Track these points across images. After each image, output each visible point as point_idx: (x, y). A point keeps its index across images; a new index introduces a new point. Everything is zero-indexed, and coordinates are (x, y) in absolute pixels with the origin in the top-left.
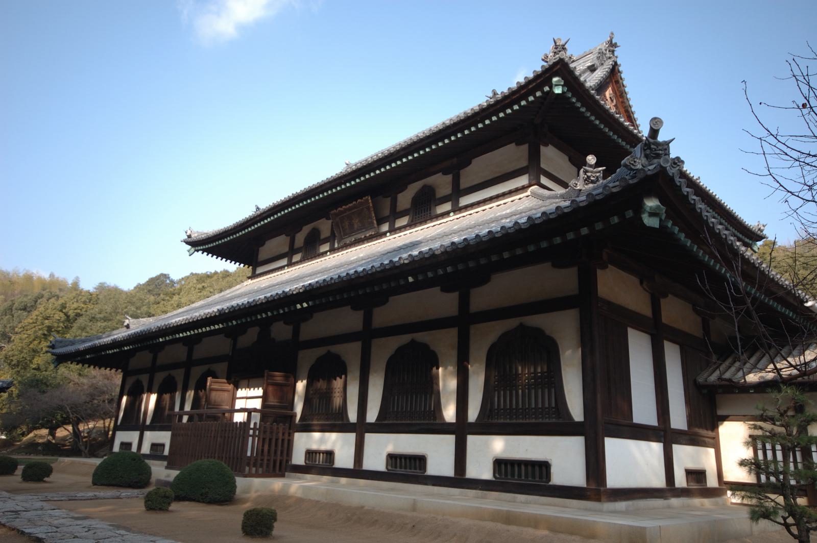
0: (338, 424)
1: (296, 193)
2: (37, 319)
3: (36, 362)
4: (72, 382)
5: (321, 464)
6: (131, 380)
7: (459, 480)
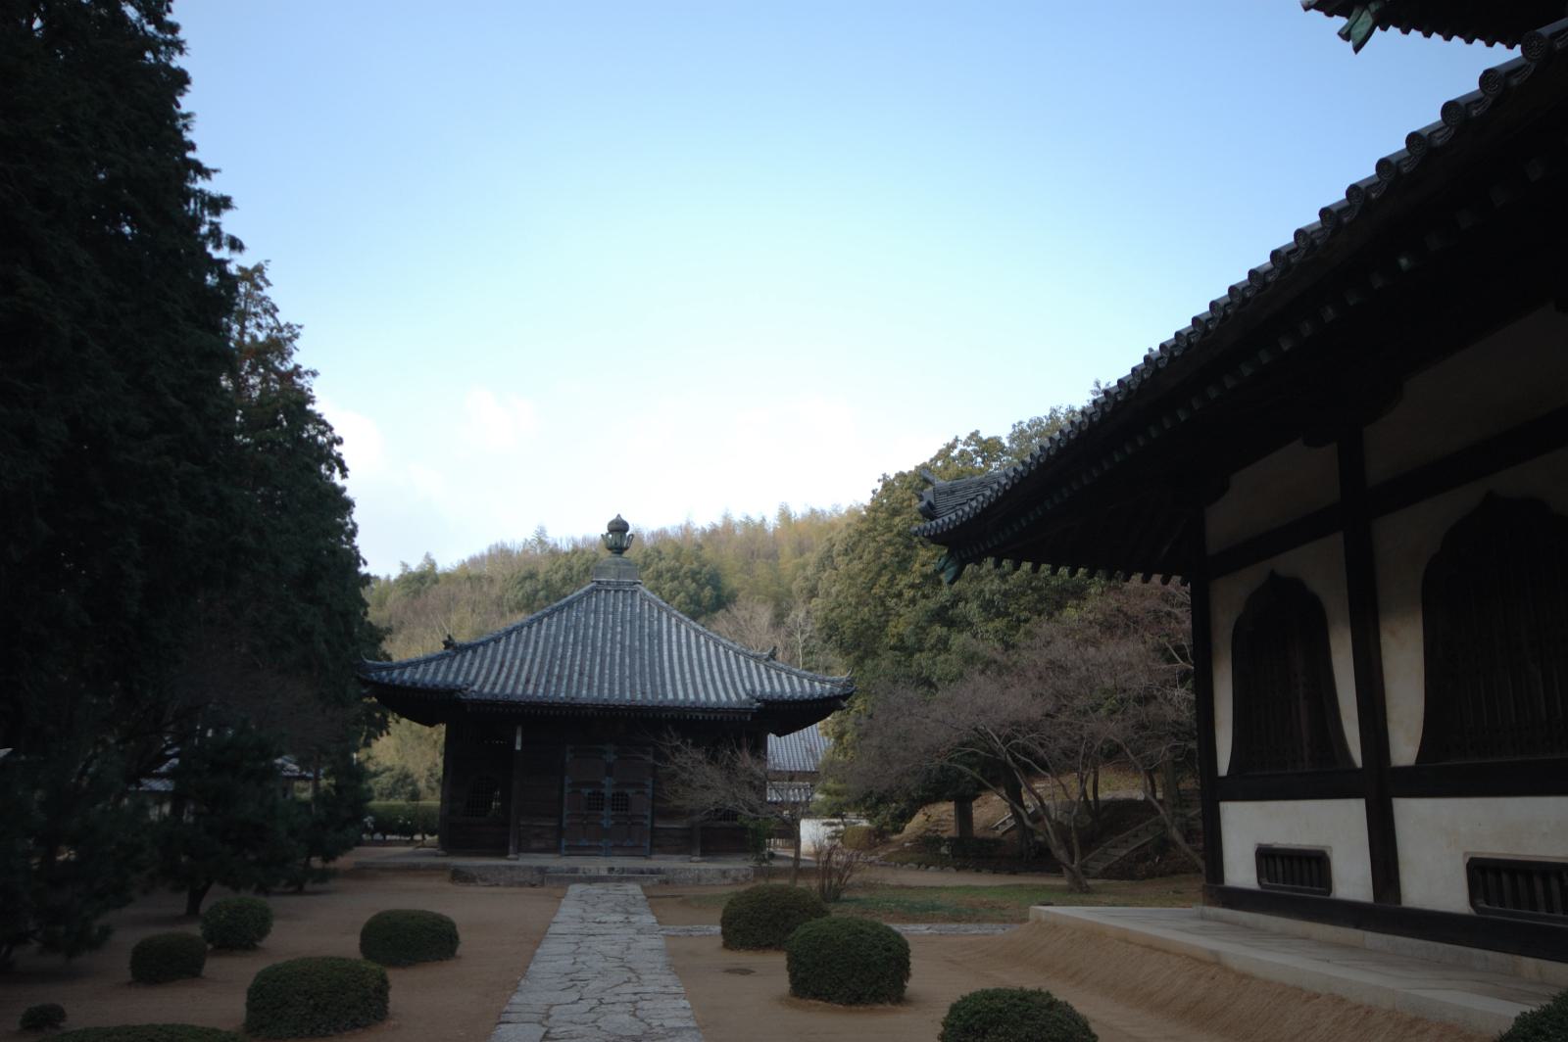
0: (1318, 775)
1: (785, 516)
2: (874, 519)
3: (895, 631)
4: (994, 666)
5: (1294, 881)
6: (1231, 599)
7: (1386, 912)
